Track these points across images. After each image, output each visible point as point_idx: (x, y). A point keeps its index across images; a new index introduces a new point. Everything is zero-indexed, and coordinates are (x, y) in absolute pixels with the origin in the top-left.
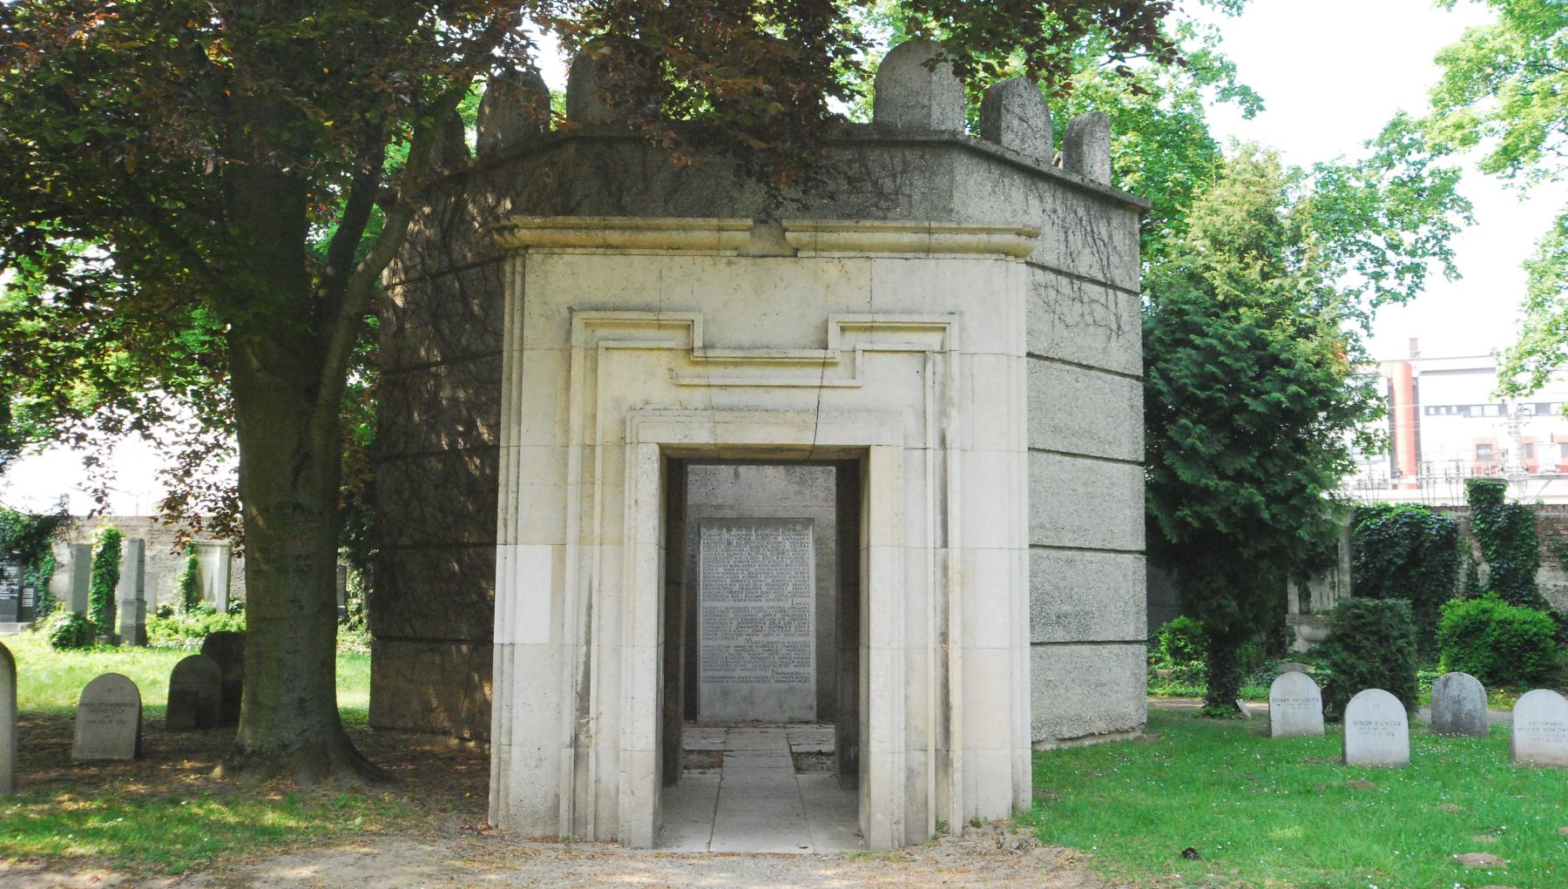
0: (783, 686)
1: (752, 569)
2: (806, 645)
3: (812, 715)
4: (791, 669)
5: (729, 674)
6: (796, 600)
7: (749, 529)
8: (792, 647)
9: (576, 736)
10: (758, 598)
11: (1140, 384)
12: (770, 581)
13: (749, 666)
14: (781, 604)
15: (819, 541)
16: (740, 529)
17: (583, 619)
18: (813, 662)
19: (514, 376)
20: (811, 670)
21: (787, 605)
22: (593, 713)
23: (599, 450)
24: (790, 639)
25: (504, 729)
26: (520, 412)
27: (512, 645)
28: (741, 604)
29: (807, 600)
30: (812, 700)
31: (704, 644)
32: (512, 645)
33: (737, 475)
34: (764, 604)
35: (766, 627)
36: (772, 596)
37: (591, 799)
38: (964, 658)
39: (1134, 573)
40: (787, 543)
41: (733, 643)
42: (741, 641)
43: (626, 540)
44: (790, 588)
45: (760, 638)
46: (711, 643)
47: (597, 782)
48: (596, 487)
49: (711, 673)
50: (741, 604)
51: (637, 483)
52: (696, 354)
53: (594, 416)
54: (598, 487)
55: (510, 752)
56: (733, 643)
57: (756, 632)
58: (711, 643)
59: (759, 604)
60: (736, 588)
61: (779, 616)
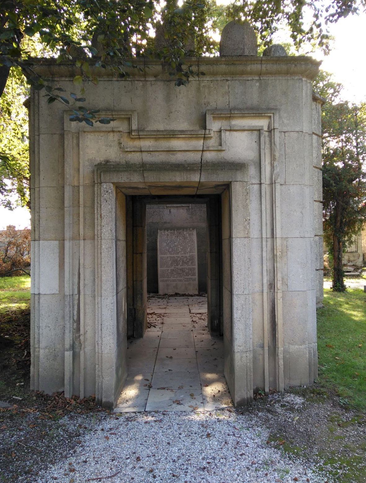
0: (187, 283)
1: (176, 244)
2: (194, 269)
3: (197, 293)
4: (190, 277)
5: (169, 279)
6: (191, 254)
7: (174, 230)
8: (190, 269)
9: (74, 343)
10: (178, 253)
11: (322, 171)
12: (182, 248)
13: (175, 276)
14: (186, 255)
15: (198, 235)
16: (171, 230)
17: (76, 280)
18: (197, 274)
19: (36, 149)
20: (196, 277)
21: (188, 255)
22: (82, 331)
23: (81, 189)
24: (189, 267)
25: (36, 340)
26: (39, 169)
27: (39, 294)
28: (172, 256)
29: (194, 254)
30: (197, 287)
31: (160, 269)
32: (39, 294)
33: (170, 212)
34: (179, 255)
35: (181, 263)
36: (182, 252)
37: (82, 379)
38: (283, 298)
39: (319, 243)
40: (187, 235)
41: (170, 269)
42: (173, 268)
43: (96, 237)
44: (189, 250)
45: (179, 267)
46: (162, 269)
47: (85, 368)
48: (81, 208)
49: (163, 279)
50: (172, 256)
51: (101, 205)
52: (133, 134)
53: (79, 170)
54: (81, 209)
55: (39, 351)
56: (170, 269)
57: (177, 265)
58: (162, 269)
59: (178, 255)
60: (170, 250)
61: (185, 259)
